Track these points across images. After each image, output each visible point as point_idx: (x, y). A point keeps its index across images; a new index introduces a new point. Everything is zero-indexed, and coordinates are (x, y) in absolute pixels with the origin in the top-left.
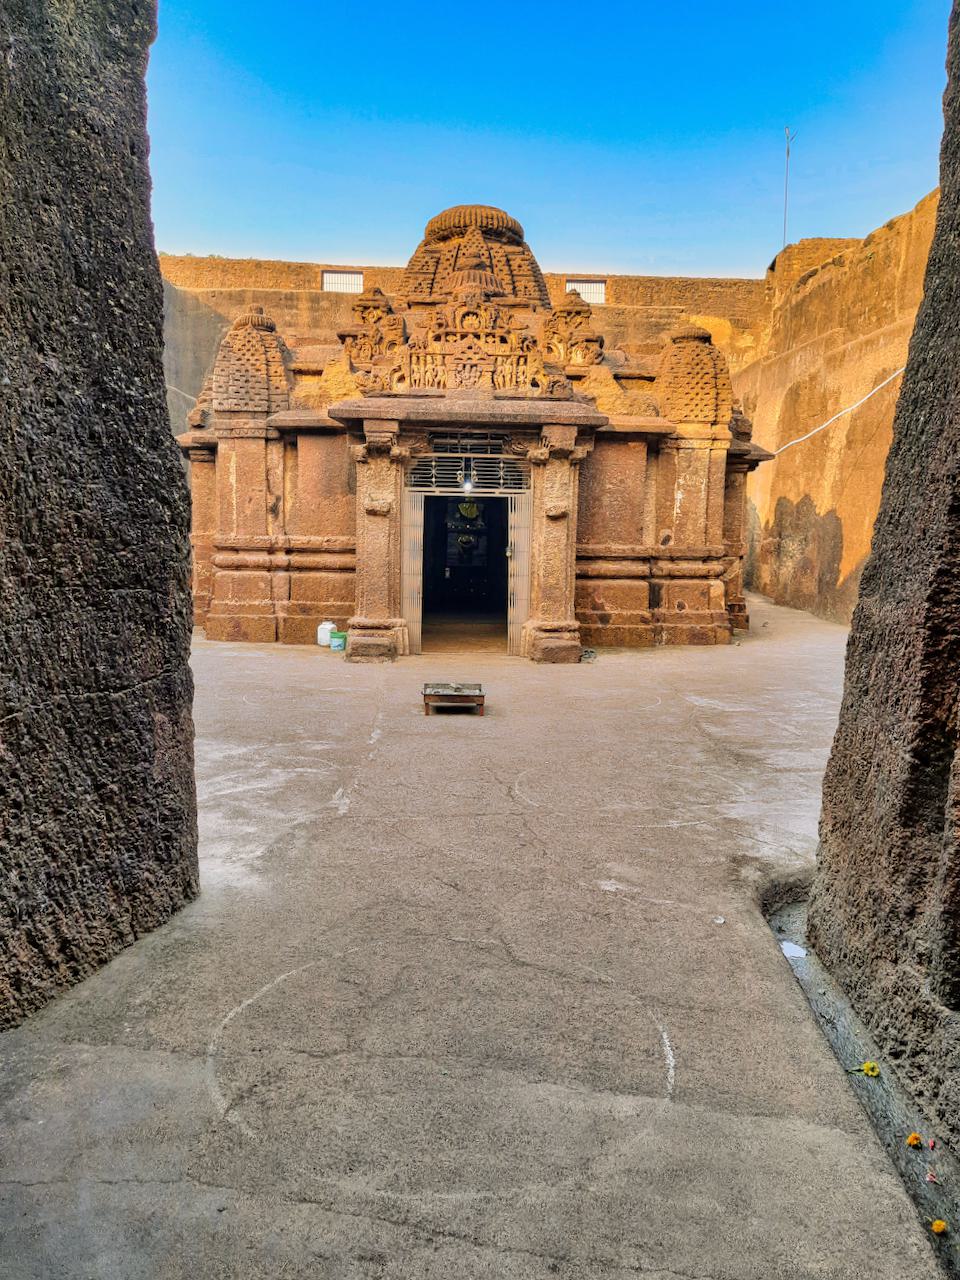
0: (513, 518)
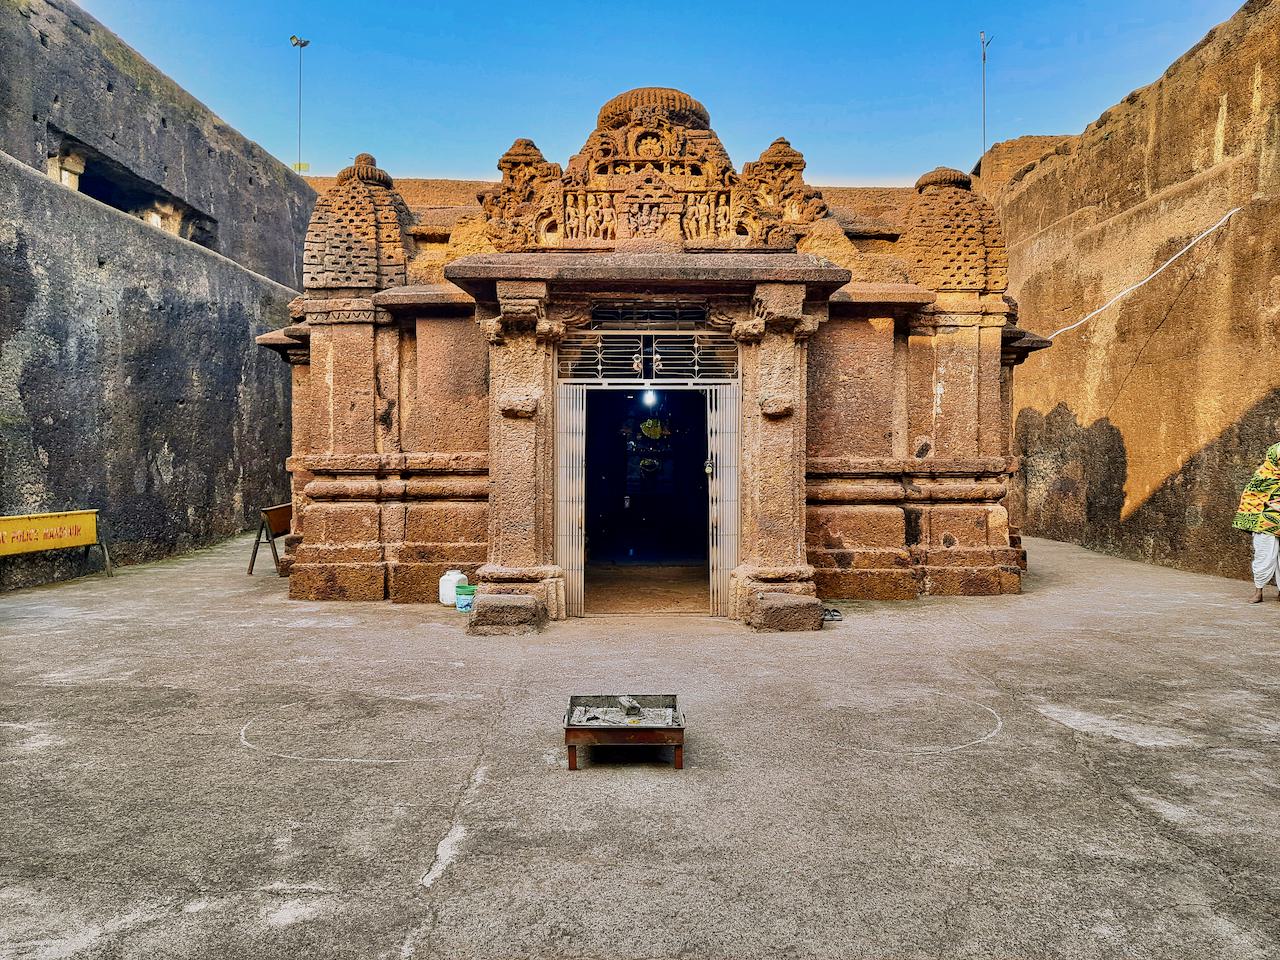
0: (713, 420)
